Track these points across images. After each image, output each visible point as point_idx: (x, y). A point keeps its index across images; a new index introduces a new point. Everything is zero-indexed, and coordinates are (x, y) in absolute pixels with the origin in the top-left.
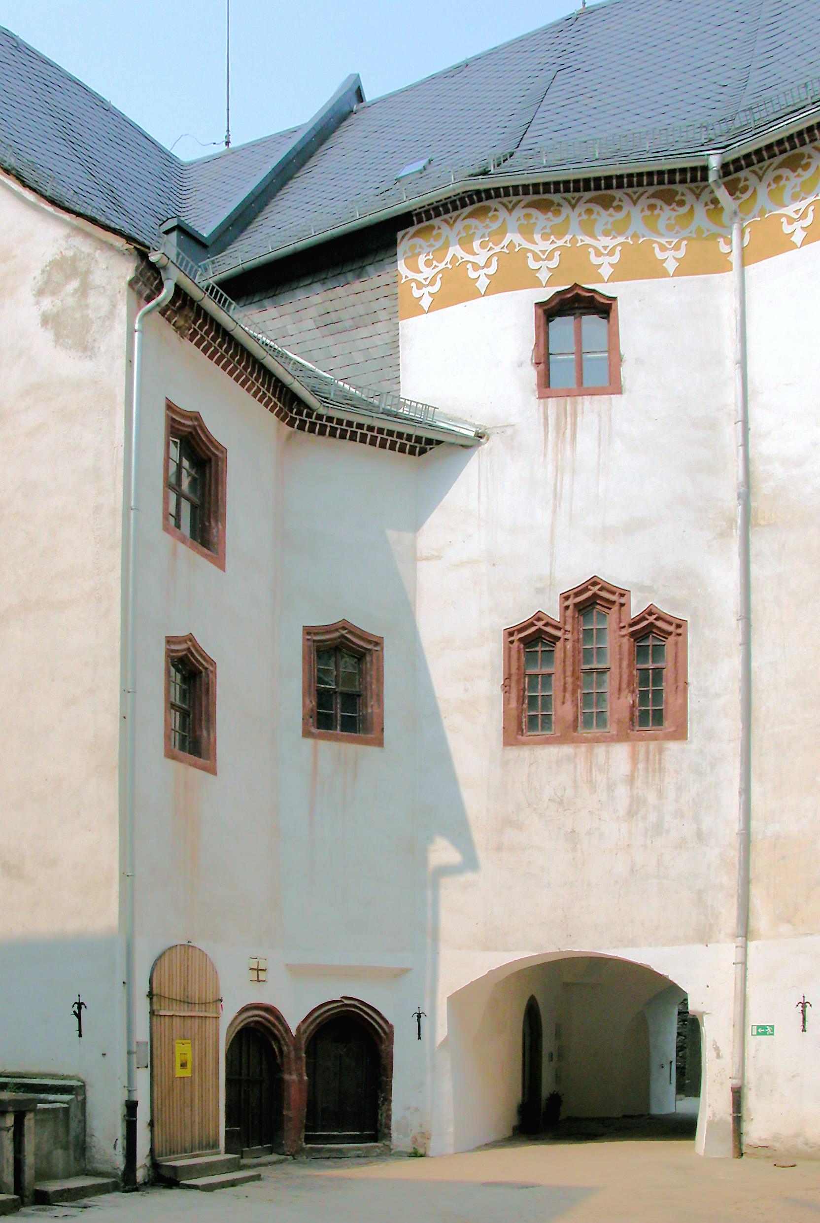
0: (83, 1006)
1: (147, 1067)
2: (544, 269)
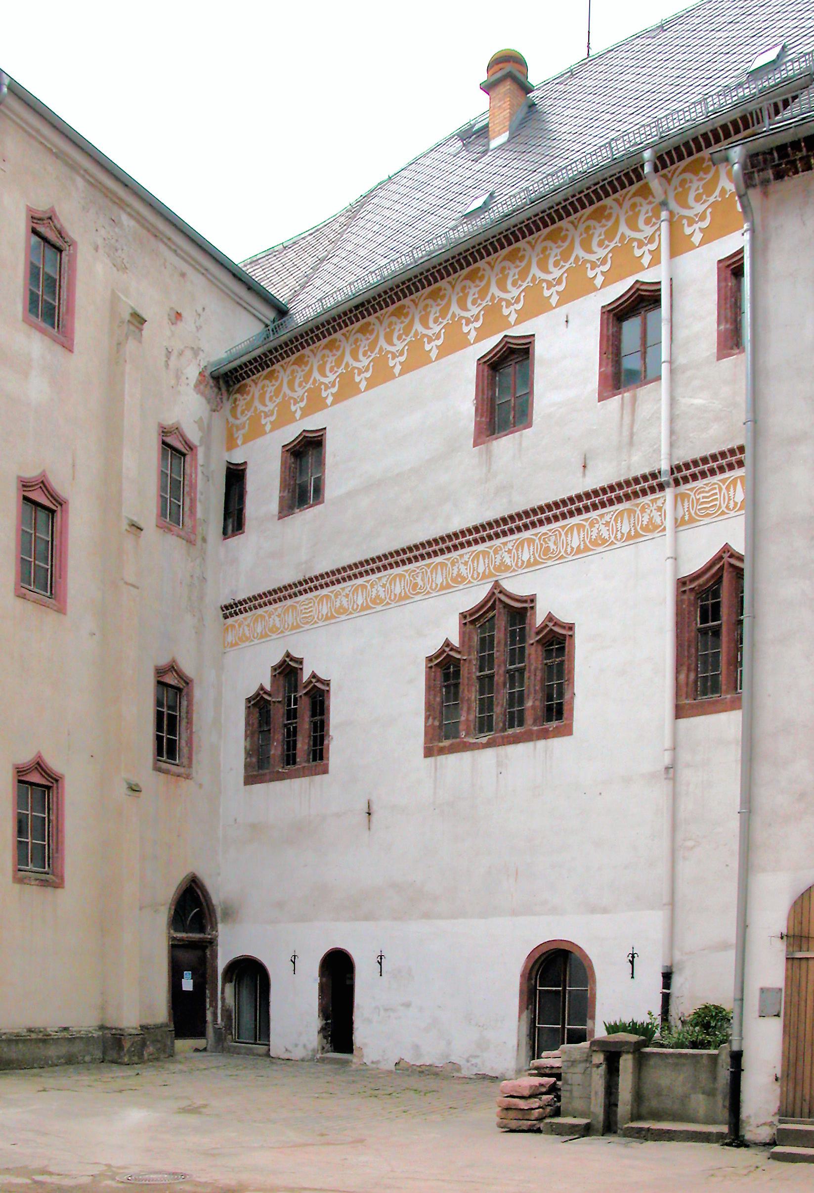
0: (635, 955)
1: (778, 1015)
2: (599, 275)
